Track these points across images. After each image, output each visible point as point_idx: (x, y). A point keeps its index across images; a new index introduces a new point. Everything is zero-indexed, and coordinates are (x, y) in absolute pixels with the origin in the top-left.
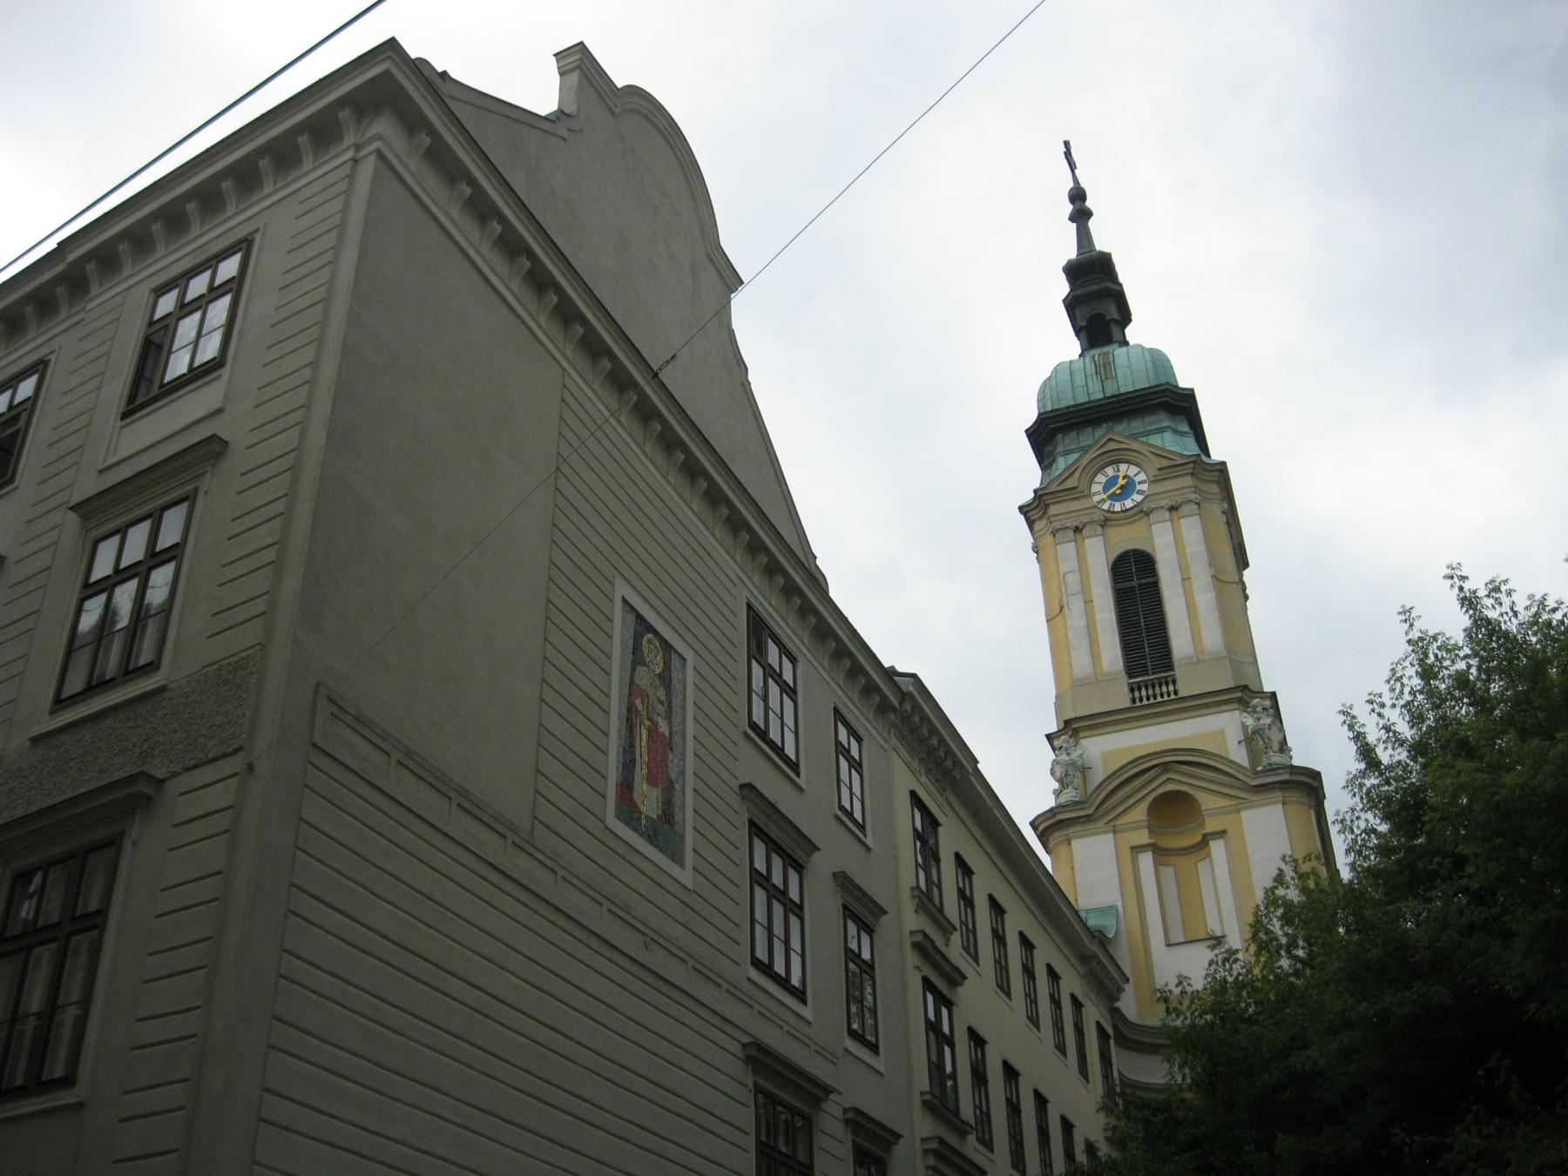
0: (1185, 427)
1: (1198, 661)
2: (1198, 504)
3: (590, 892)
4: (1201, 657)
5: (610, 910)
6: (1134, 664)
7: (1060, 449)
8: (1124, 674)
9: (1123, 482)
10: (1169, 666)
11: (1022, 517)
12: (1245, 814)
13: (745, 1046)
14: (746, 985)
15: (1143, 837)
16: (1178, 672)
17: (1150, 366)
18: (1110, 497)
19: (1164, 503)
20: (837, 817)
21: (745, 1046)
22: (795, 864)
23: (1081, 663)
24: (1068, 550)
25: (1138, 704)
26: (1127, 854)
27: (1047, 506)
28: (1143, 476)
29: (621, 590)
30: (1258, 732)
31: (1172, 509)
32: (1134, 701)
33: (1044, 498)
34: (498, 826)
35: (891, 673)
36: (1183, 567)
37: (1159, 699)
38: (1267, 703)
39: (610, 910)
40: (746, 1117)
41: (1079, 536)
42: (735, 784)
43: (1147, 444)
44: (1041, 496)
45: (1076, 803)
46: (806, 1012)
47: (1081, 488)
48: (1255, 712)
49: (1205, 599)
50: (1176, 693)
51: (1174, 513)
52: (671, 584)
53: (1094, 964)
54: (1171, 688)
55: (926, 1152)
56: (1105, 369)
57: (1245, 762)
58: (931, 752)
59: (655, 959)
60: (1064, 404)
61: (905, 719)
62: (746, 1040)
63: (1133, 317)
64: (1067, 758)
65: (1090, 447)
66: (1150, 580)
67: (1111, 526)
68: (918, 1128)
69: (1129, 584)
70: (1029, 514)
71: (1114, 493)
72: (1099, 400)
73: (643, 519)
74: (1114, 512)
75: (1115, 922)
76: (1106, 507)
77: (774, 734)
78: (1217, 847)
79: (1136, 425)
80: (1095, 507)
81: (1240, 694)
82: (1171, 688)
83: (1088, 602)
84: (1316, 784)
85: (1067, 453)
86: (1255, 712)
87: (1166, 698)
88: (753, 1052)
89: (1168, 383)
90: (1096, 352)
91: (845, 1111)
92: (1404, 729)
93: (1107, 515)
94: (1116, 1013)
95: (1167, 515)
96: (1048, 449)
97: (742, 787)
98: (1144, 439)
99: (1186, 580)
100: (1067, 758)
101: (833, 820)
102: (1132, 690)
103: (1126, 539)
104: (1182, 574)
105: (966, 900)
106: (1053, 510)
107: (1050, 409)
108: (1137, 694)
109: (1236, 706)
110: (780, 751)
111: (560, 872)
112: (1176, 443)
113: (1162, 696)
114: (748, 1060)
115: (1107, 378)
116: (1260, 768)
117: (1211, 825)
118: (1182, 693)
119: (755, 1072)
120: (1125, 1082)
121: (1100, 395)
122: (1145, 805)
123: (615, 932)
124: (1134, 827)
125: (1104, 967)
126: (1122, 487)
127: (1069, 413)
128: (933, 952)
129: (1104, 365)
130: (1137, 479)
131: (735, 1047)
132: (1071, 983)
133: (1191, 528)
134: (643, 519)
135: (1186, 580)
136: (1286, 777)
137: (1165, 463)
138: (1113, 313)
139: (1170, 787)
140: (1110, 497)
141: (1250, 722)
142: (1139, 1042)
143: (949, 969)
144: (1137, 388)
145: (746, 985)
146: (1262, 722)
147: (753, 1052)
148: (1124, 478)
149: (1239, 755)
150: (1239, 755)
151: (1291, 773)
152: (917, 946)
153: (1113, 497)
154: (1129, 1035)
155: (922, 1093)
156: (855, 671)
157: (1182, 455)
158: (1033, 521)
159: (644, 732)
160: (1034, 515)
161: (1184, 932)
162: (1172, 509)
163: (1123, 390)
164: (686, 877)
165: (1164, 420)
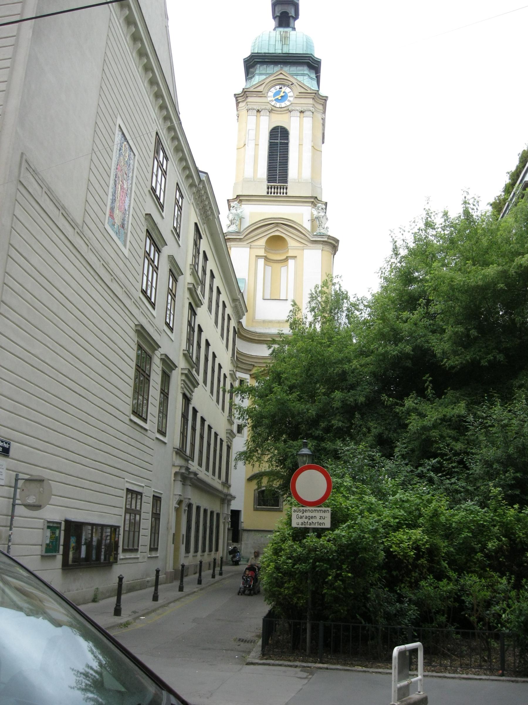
0: (313, 76)
1: (299, 182)
2: (313, 113)
3: (98, 256)
4: (300, 180)
5: (103, 264)
6: (271, 178)
7: (257, 72)
8: (266, 180)
9: (283, 94)
10: (286, 181)
11: (234, 99)
12: (306, 252)
13: (136, 325)
14: (138, 300)
15: (262, 252)
16: (289, 184)
17: (305, 43)
18: (275, 100)
19: (300, 109)
20: (172, 231)
21: (136, 325)
22: (158, 250)
23: (249, 173)
24: (252, 119)
25: (269, 195)
26: (254, 258)
27: (247, 97)
28: (291, 94)
29: (119, 121)
30: (318, 218)
31: (302, 112)
32: (268, 193)
33: (247, 93)
34: (73, 224)
35: (198, 171)
36: (301, 139)
37: (279, 195)
38: (324, 207)
39: (103, 264)
40: (133, 354)
41: (258, 114)
42: (144, 213)
43: (296, 79)
44: (246, 91)
45: (237, 232)
46: (154, 313)
47: (263, 93)
48: (318, 209)
49: (307, 154)
50: (286, 193)
51: (302, 114)
52: (134, 121)
53: (237, 303)
54: (285, 191)
55: (182, 374)
56: (284, 39)
57: (309, 229)
58: (204, 207)
59: (114, 286)
60: (263, 51)
61: (198, 191)
62: (137, 323)
63: (300, 17)
64: (235, 212)
65: (272, 74)
66: (286, 141)
67: (274, 113)
68: (181, 364)
69: (276, 141)
70: (238, 98)
71: (278, 99)
72: (280, 54)
73: (129, 88)
74: (276, 107)
75: (244, 286)
76: (273, 103)
77: (158, 193)
78: (291, 262)
79: (293, 69)
80: (268, 103)
81: (313, 200)
82: (285, 191)
83: (257, 145)
84: (336, 245)
85: (261, 74)
86: (318, 209)
87: (282, 195)
88: (139, 328)
89: (312, 54)
90: (282, 29)
91: (161, 355)
92: (412, 245)
93: (273, 107)
94: (240, 323)
95: (299, 114)
96: (251, 70)
97: (146, 214)
98: (295, 77)
99: (301, 145)
100: (235, 212)
101: (170, 232)
102: (268, 188)
103: (279, 120)
104: (299, 142)
105: (204, 271)
106: (250, 99)
107: (256, 52)
108: (270, 190)
109: (310, 204)
110: (158, 199)
111: (90, 246)
112: (309, 82)
113: (280, 193)
114: (137, 331)
115: (285, 44)
116: (315, 234)
117: (291, 253)
118: (288, 194)
119: (138, 337)
120: (239, 353)
121: (280, 52)
122: (265, 239)
123: (102, 272)
124: (259, 247)
125: (241, 305)
126: (282, 97)
127: (265, 56)
128: (194, 293)
129: (285, 37)
130: (289, 95)
131: (133, 326)
132: (229, 310)
133: (308, 122)
134: (129, 88)
135: (301, 145)
136: (326, 239)
137: (303, 91)
138: (292, 13)
139: (277, 233)
140: (275, 100)
141: (315, 213)
142: (245, 337)
143: (197, 299)
144: (297, 52)
145: (138, 300)
146: (320, 214)
147: (139, 328)
148: (284, 92)
149: (307, 225)
150: (307, 225)
151: (328, 238)
152: (189, 289)
153: (277, 100)
154: (242, 333)
155: (184, 350)
156: (186, 168)
157: (311, 89)
158: (239, 102)
159: (119, 186)
160: (240, 99)
161: (271, 295)
162: (302, 112)
163: (291, 52)
164: (126, 252)
165: (305, 70)
